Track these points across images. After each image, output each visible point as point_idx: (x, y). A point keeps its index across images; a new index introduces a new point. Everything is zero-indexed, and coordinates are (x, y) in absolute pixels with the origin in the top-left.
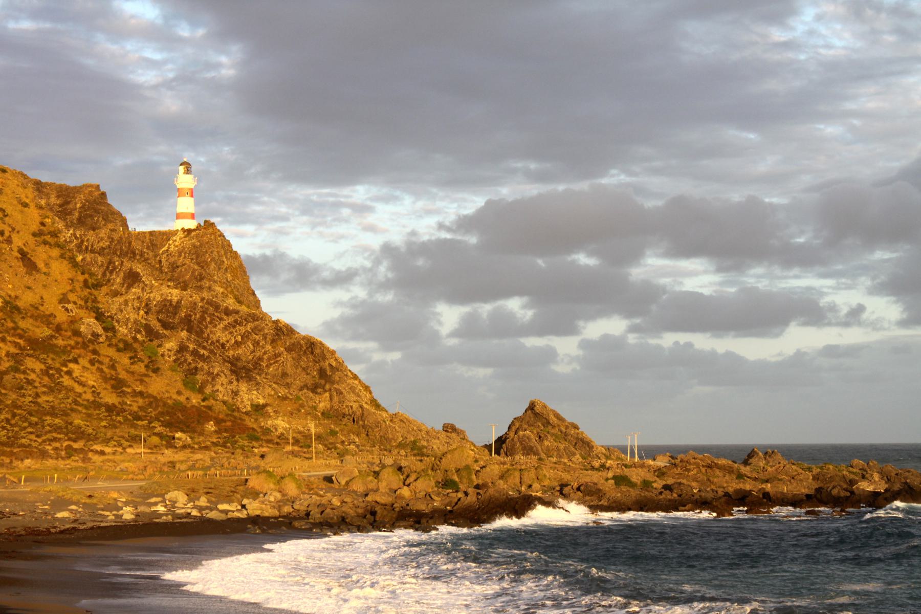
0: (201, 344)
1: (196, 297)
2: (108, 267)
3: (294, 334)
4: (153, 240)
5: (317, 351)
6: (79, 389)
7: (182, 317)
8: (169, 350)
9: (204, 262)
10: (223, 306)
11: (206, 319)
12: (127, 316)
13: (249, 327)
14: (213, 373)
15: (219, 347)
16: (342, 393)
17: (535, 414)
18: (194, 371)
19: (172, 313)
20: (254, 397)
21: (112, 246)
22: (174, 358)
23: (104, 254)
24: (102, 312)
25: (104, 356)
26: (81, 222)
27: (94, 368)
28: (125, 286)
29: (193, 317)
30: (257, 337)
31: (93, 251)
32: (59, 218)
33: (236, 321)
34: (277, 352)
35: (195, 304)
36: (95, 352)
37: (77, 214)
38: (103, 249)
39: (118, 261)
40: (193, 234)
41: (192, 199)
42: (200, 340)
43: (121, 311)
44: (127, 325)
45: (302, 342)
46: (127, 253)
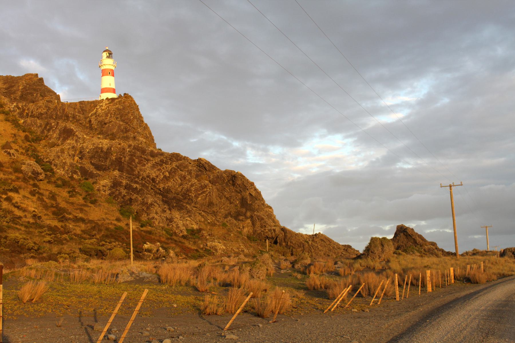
0: (133, 179)
1: (124, 144)
2: (45, 127)
3: (215, 170)
4: (83, 107)
5: (239, 182)
6: (18, 213)
7: (113, 160)
8: (103, 186)
9: (127, 119)
10: (148, 150)
11: (134, 160)
12: (64, 161)
13: (174, 165)
14: (147, 203)
15: (150, 182)
16: (263, 219)
17: (406, 236)
18: (129, 202)
19: (104, 158)
20: (188, 222)
21: (49, 113)
22: (109, 192)
23: (42, 119)
24: (41, 158)
25: (43, 189)
26: (23, 98)
27: (35, 198)
28: (61, 139)
29: (123, 159)
30: (183, 173)
31: (32, 116)
32: (5, 96)
33: (162, 161)
34: (203, 184)
35: (124, 149)
36: (35, 185)
37: (20, 93)
38: (41, 114)
39: (54, 122)
40: (116, 101)
41: (112, 78)
42: (133, 177)
43: (59, 157)
44: (64, 168)
45: (224, 175)
46: (62, 116)
